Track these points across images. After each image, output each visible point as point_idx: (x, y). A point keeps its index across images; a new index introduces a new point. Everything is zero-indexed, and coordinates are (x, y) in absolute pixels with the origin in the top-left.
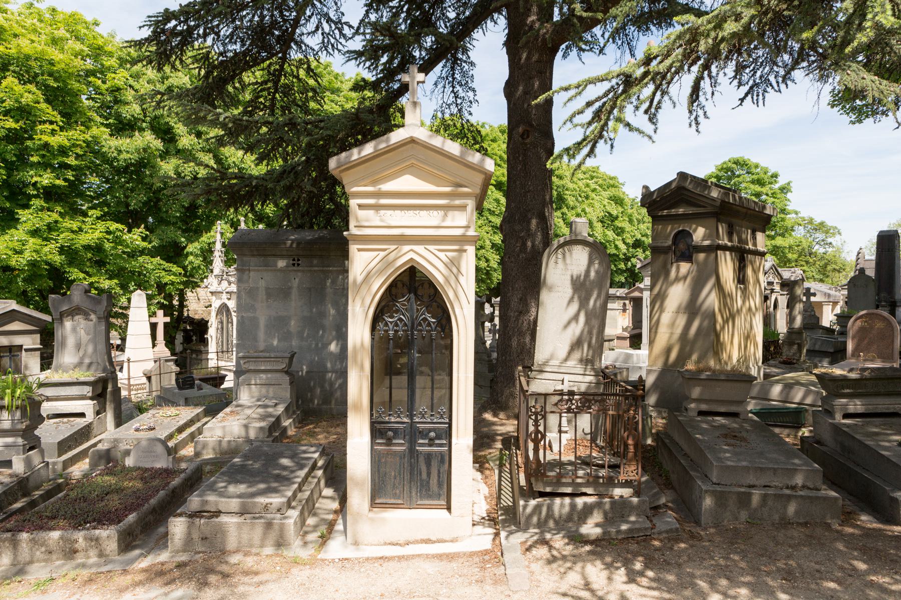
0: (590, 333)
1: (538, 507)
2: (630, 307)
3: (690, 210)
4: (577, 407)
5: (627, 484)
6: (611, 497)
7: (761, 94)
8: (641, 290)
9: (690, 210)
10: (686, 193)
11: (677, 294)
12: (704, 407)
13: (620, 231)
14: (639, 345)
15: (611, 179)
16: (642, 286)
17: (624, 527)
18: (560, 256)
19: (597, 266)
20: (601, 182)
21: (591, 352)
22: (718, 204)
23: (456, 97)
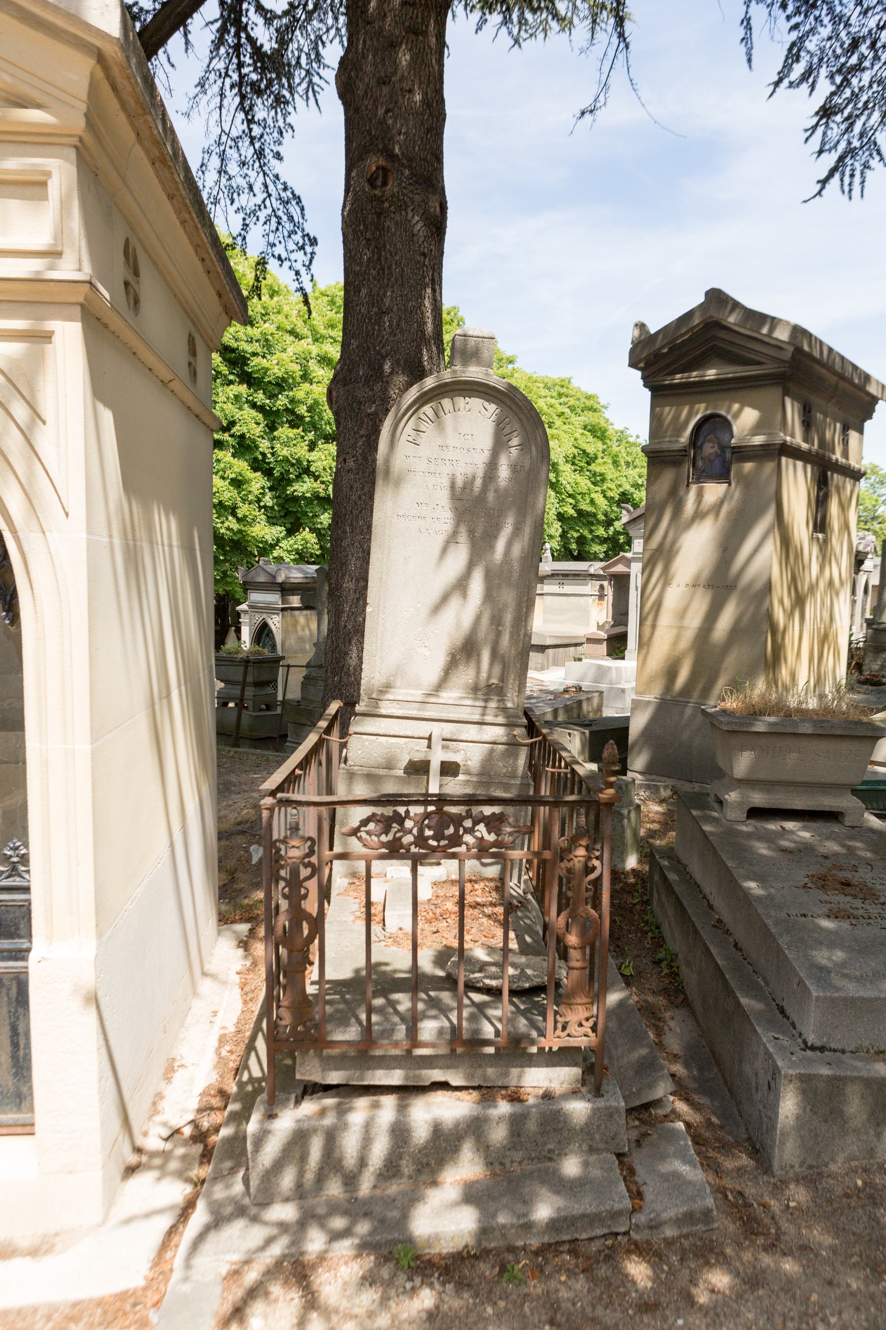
0: (496, 621)
1: (299, 1139)
2: (609, 591)
3: (732, 371)
4: (421, 840)
5: (563, 1056)
6: (515, 1098)
7: (858, 173)
8: (628, 562)
9: (732, 371)
10: (722, 334)
11: (696, 547)
12: (758, 799)
13: (598, 479)
14: (623, 651)
15: (589, 397)
16: (629, 555)
17: (543, 1211)
19: (514, 452)
20: (572, 402)
21: (497, 670)
22: (788, 355)
23: (250, 122)
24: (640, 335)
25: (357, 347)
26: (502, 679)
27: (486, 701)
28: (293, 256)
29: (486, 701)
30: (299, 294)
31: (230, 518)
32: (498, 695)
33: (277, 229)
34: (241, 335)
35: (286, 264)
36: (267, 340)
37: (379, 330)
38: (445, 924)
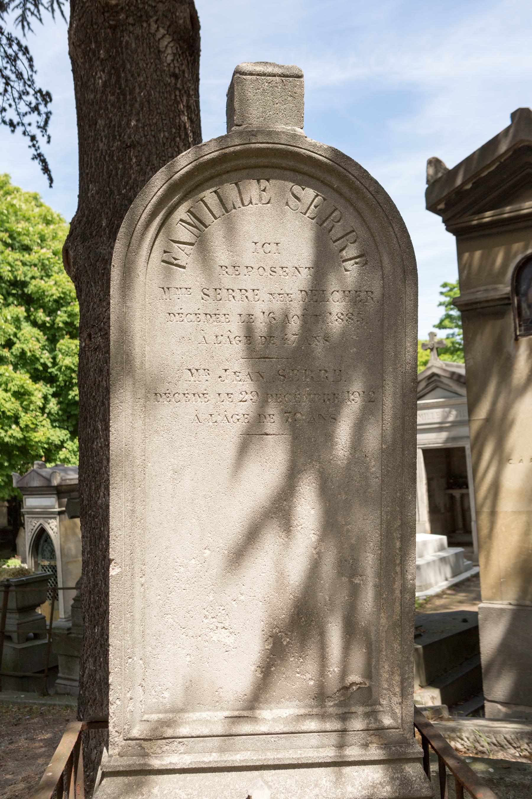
0: (349, 568)
18: (183, 233)
19: (351, 271)
21: (358, 659)
24: (436, 172)
25: (97, 193)
26: (369, 672)
27: (344, 717)
28: (26, 120)
29: (344, 717)
30: (37, 161)
31: (14, 426)
33: (6, 91)
35: (19, 129)
36: (43, 265)
37: (124, 168)
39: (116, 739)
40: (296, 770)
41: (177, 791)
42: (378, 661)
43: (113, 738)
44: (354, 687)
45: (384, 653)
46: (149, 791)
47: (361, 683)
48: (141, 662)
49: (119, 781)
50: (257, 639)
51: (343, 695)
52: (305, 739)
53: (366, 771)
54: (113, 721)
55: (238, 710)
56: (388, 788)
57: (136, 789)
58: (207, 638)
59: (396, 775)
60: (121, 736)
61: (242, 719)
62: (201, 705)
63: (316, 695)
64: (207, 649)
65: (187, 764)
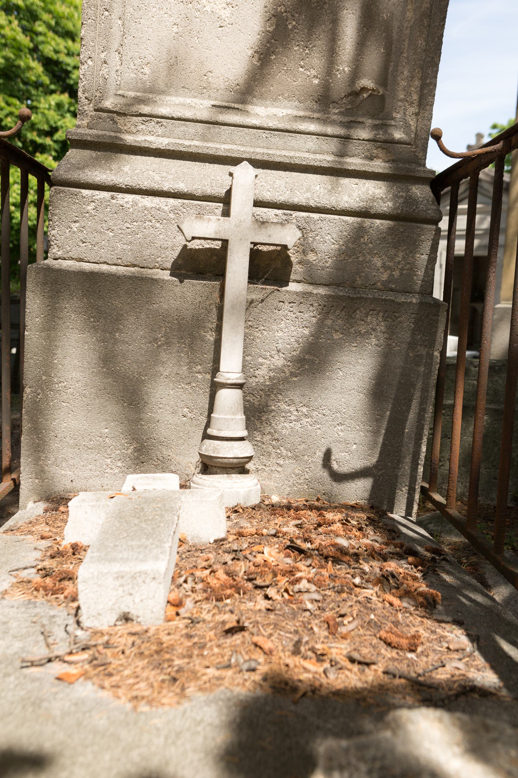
21: (373, 60)
26: (385, 78)
29: (350, 125)
32: (373, 117)
34: (62, 47)
38: (263, 604)
39: (86, 108)
40: (287, 173)
41: (151, 172)
42: (397, 66)
43: (81, 106)
44: (365, 95)
45: (405, 55)
46: (119, 168)
47: (373, 90)
48: (120, 22)
49: (85, 154)
50: (258, 16)
51: (352, 102)
52: (302, 141)
53: (367, 185)
54: (83, 84)
55: (227, 102)
56: (390, 204)
57: (105, 163)
58: (199, 6)
59: (401, 194)
60: (91, 105)
61: (231, 111)
62: (186, 90)
63: (320, 98)
64: (198, 20)
65: (164, 144)
